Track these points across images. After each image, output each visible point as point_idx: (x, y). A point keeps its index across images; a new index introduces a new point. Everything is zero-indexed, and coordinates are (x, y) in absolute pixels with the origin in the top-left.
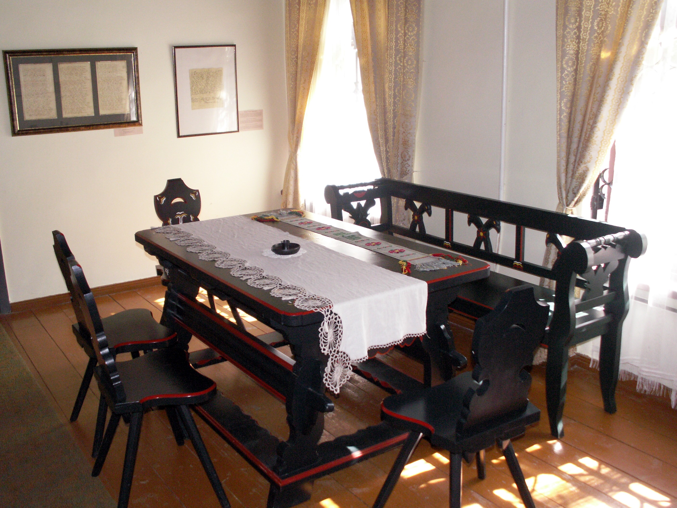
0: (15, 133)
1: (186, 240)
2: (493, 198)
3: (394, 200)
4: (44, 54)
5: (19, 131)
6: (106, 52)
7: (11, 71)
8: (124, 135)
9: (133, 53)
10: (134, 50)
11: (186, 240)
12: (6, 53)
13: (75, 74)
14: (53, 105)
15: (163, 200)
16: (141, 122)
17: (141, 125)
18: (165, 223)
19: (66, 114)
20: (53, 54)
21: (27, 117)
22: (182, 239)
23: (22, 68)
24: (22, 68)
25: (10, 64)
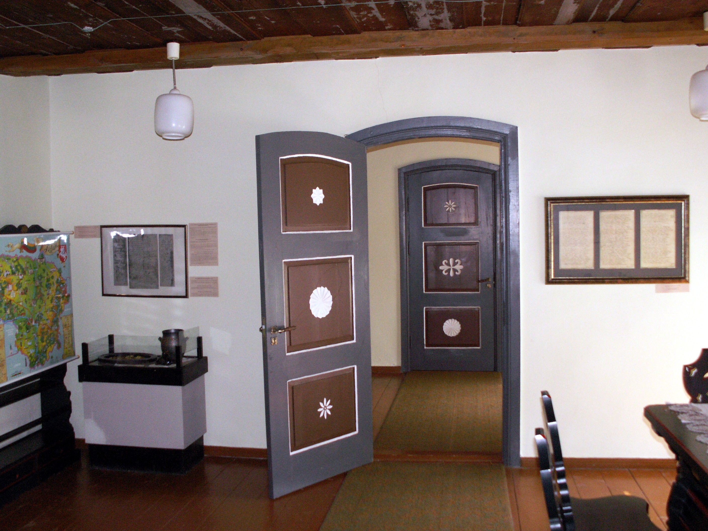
0: (549, 281)
1: (702, 425)
2: (486, 53)
3: (36, 399)
4: (586, 201)
5: (553, 279)
6: (653, 200)
7: (551, 218)
8: (666, 292)
9: (684, 201)
10: (685, 198)
11: (702, 425)
12: (548, 200)
13: (618, 223)
14: (591, 255)
15: (694, 372)
16: (689, 280)
17: (688, 282)
18: (694, 400)
19: (604, 265)
20: (595, 202)
21: (563, 266)
22: (697, 423)
23: (563, 215)
24: (563, 215)
25: (551, 210)
